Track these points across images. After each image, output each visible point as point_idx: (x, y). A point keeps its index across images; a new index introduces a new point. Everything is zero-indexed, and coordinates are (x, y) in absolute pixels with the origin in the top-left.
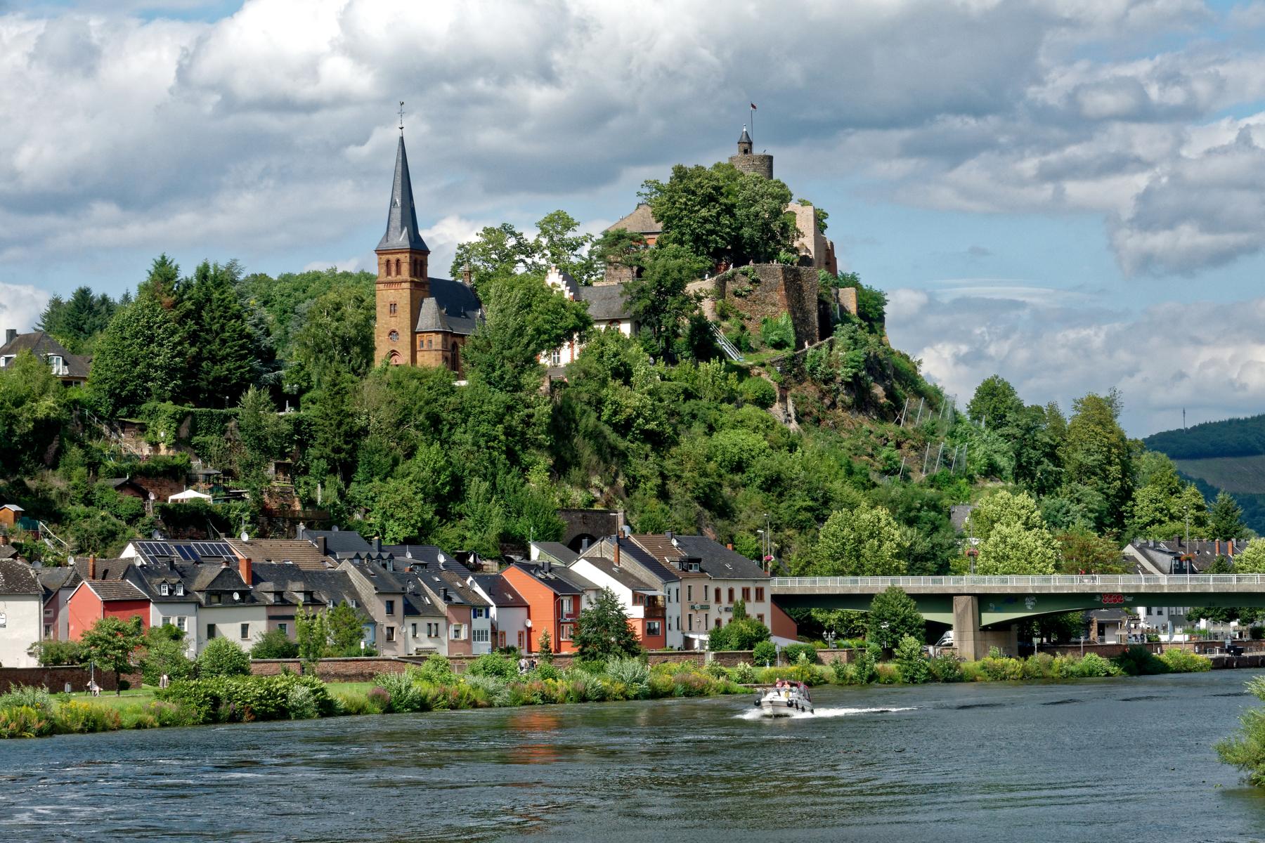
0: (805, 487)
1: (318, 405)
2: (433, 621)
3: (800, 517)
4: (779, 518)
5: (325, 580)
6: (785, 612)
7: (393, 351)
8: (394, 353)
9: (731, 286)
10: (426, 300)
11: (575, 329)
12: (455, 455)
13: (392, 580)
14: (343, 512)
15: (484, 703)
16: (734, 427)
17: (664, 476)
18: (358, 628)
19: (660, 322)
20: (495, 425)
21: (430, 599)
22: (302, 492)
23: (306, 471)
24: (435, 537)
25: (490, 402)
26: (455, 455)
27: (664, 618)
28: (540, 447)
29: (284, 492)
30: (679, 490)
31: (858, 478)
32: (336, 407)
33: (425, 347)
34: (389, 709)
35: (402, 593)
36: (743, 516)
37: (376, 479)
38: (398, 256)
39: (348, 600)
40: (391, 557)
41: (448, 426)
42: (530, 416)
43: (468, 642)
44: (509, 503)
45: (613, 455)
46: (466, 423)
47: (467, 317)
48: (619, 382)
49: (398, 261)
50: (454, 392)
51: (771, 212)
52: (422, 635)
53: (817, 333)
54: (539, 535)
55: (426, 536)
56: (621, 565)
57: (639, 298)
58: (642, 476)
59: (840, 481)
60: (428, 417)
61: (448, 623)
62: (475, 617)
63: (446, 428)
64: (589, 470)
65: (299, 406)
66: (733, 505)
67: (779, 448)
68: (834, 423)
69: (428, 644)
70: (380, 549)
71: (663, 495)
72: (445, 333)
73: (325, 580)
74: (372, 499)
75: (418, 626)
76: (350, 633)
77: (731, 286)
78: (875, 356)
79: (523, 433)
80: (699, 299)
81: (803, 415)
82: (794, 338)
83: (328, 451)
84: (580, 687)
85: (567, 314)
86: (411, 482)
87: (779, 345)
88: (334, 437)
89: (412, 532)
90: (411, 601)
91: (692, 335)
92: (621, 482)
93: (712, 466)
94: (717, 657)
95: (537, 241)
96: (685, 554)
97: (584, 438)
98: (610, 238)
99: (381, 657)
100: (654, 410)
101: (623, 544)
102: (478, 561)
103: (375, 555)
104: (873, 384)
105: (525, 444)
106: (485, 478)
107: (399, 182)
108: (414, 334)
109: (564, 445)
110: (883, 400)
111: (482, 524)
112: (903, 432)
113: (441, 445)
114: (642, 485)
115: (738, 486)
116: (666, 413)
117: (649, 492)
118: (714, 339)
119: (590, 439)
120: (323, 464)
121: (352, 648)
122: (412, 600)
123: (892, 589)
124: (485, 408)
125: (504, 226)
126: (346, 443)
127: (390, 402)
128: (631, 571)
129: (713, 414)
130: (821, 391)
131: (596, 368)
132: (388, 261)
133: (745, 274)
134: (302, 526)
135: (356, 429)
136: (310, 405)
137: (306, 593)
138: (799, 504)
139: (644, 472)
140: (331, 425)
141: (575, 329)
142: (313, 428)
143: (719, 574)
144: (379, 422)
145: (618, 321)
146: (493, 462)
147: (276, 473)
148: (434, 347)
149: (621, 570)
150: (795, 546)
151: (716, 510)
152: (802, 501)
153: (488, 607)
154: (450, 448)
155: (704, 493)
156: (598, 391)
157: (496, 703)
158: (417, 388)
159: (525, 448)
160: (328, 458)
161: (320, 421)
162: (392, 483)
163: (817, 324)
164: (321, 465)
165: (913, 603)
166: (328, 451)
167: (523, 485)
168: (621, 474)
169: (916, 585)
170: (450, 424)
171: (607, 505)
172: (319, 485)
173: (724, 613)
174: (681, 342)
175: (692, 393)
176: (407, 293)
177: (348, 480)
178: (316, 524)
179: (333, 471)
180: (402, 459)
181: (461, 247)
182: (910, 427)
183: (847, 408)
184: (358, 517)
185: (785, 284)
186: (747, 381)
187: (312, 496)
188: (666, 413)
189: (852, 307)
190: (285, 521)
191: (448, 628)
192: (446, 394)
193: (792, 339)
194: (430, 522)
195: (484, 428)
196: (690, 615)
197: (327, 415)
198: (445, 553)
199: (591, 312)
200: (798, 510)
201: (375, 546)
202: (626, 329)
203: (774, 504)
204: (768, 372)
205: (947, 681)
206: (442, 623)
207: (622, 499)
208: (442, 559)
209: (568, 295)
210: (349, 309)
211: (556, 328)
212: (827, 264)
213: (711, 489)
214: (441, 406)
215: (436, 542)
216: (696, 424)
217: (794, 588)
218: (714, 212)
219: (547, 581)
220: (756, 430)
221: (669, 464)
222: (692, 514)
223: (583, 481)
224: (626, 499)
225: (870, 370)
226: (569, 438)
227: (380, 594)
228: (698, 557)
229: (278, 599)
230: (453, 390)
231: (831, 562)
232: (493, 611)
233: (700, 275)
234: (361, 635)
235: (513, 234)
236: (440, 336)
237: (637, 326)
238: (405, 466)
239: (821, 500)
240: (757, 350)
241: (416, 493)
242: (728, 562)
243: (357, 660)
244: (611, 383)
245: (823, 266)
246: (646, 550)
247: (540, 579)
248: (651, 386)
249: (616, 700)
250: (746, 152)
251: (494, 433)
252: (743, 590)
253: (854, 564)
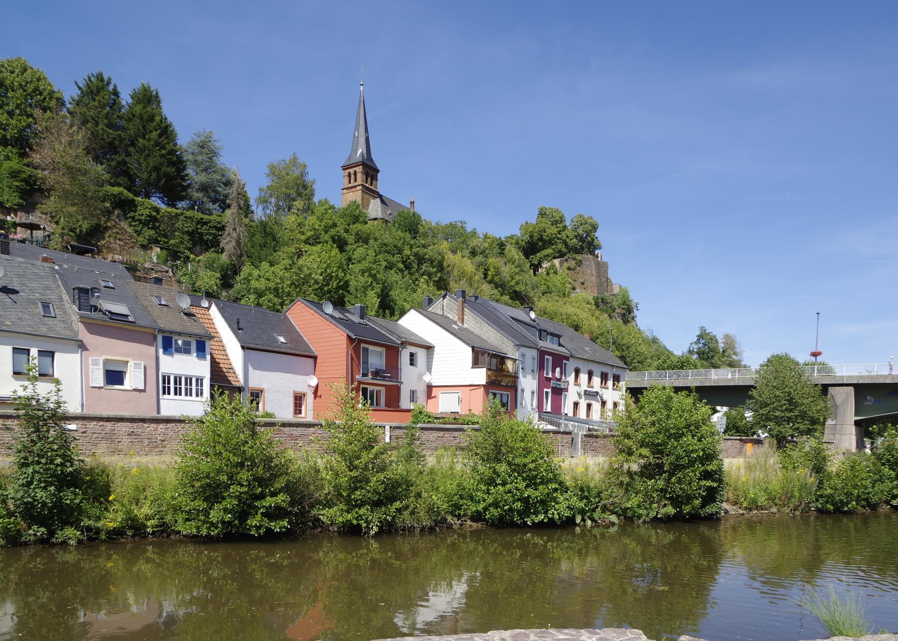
38: (355, 169)
56: (465, 326)
132: (349, 173)
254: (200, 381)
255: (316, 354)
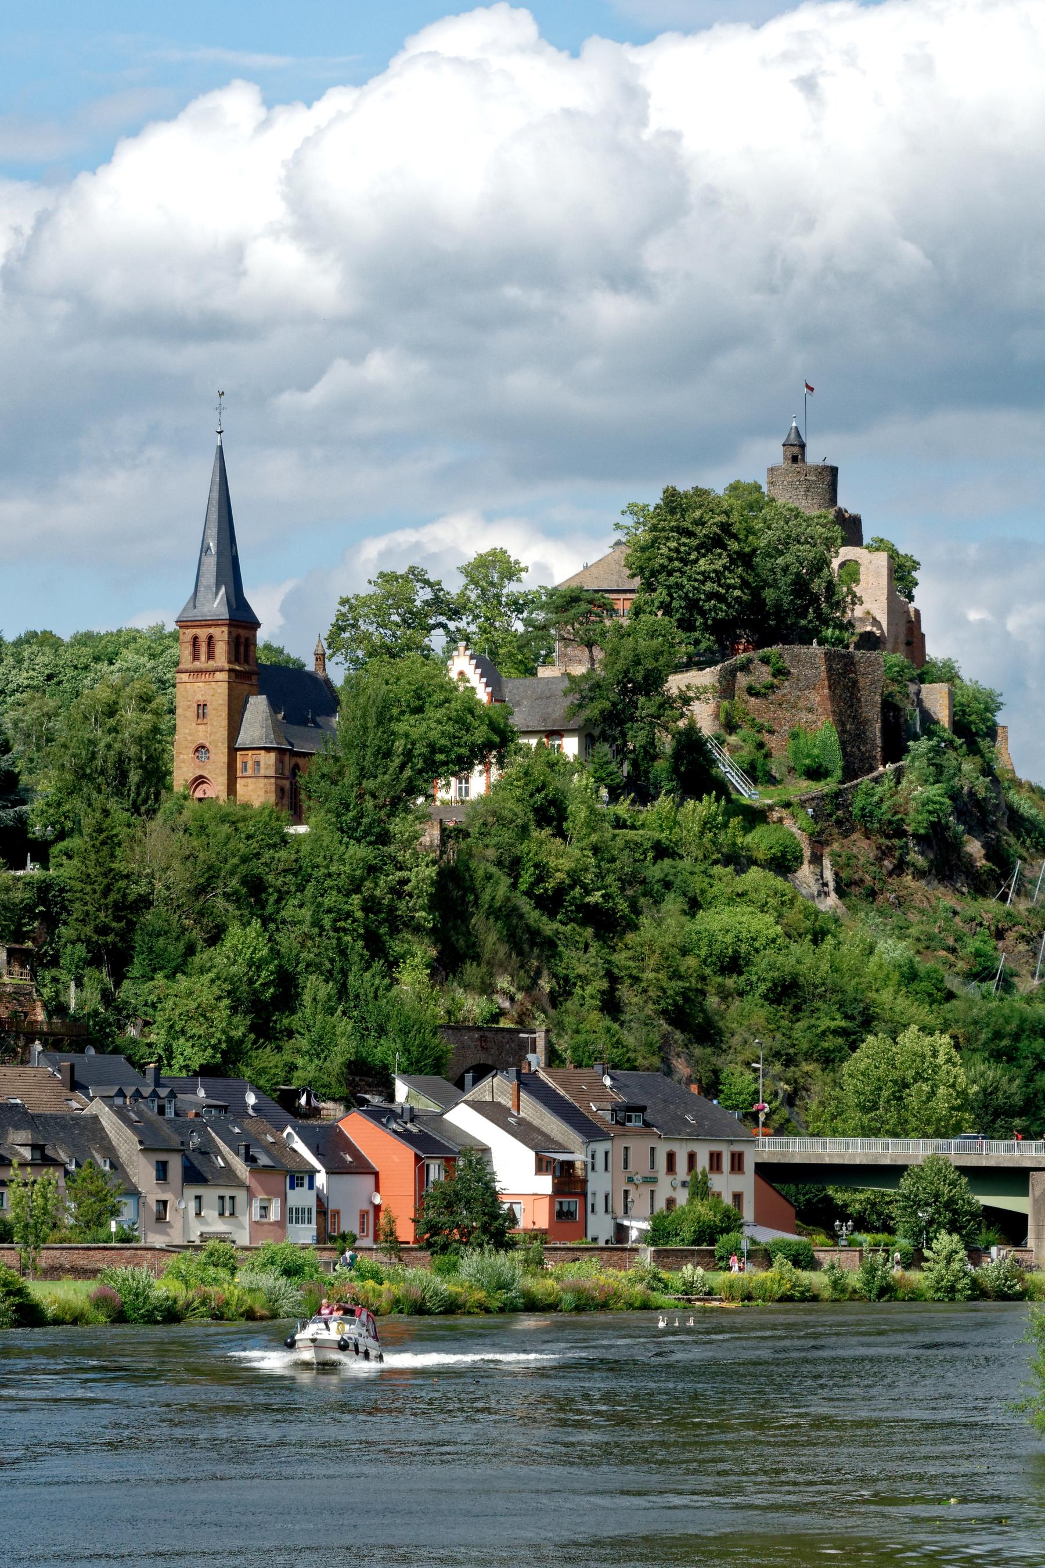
0: (836, 998)
1: (76, 862)
2: (227, 1193)
3: (826, 1045)
4: (793, 1046)
5: (64, 1127)
6: (774, 1188)
7: (201, 777)
8: (200, 780)
9: (743, 680)
10: (252, 700)
11: (489, 746)
12: (287, 940)
13: (166, 1130)
14: (110, 1025)
15: (265, 1312)
16: (731, 901)
17: (613, 979)
18: (111, 1200)
19: (623, 734)
20: (348, 895)
21: (224, 1159)
22: (47, 992)
23: (55, 962)
24: (247, 1066)
25: (341, 860)
26: (287, 940)
27: (584, 1194)
28: (418, 929)
29: (19, 993)
30: (635, 1000)
31: (925, 986)
32: (101, 865)
33: (249, 772)
34: (120, 1317)
35: (181, 1150)
36: (736, 1041)
37: (160, 975)
38: (211, 630)
39: (100, 1160)
40: (172, 1095)
41: (276, 896)
42: (405, 882)
43: (280, 1224)
44: (367, 1015)
45: (533, 944)
46: (302, 891)
47: (318, 726)
48: (548, 831)
49: (210, 638)
50: (286, 842)
51: (812, 565)
52: (210, 1213)
53: (879, 756)
54: (411, 1064)
55: (234, 1063)
56: (522, 1114)
57: (592, 699)
58: (579, 976)
59: (891, 989)
60: (244, 882)
61: (251, 1195)
62: (292, 1187)
63: (272, 899)
64: (493, 967)
65: (48, 861)
66: (721, 1024)
67: (800, 935)
68: (897, 898)
69: (219, 1226)
70: (158, 1083)
71: (611, 1006)
72: (280, 751)
73: (64, 1127)
74: (154, 1006)
75: (204, 1200)
76: (97, 1207)
77: (743, 680)
78: (972, 794)
79: (392, 909)
80: (687, 701)
81: (848, 885)
82: (841, 763)
83: (88, 930)
84: (416, 1293)
85: (476, 724)
86: (213, 981)
87: (815, 773)
88: (99, 910)
89: (213, 1057)
90: (196, 1163)
91: (677, 756)
92: (546, 985)
93: (691, 961)
94: (659, 1255)
95: (462, 594)
96: (622, 1099)
97: (487, 918)
98: (560, 602)
99: (142, 1244)
100: (600, 876)
101: (527, 1083)
102: (314, 1102)
103: (147, 1091)
104: (966, 837)
105: (396, 924)
106: (329, 976)
107: (214, 516)
108: (233, 751)
109: (455, 928)
110: (981, 863)
111: (320, 1048)
112: (1009, 914)
113: (264, 924)
114: (577, 990)
115: (731, 995)
116: (620, 879)
117: (589, 1002)
118: (713, 762)
119: (497, 919)
120: (81, 950)
121: (100, 1230)
122: (197, 1161)
123: (934, 1159)
124: (333, 869)
125: (412, 570)
126: (118, 919)
127: (187, 858)
128: (536, 1122)
129: (698, 883)
130: (879, 848)
131: (511, 810)
132: (195, 638)
133: (765, 661)
134: (38, 1046)
135: (131, 898)
136: (64, 860)
137: (34, 1147)
138: (825, 1023)
139: (582, 970)
140: (95, 892)
141: (489, 746)
142: (68, 896)
143: (674, 1129)
144: (168, 888)
145: (559, 733)
146: (343, 953)
147: (9, 963)
148: (262, 772)
149: (522, 1122)
150: (815, 1088)
151: (693, 1032)
152: (830, 1020)
153: (312, 1173)
154: (278, 929)
155: (675, 1004)
156: (513, 845)
157: (281, 1312)
158: (228, 838)
159: (394, 931)
160: (88, 941)
161: (79, 886)
162: (183, 983)
163: (879, 742)
164: (78, 953)
165: (964, 1180)
166: (88, 930)
167: (389, 988)
168: (545, 972)
169: (901, 1152)
170: (279, 891)
171: (520, 1021)
172: (72, 984)
173: (680, 1189)
174: (661, 766)
175: (667, 848)
176: (223, 689)
177: (119, 977)
178: (66, 1042)
179: (95, 962)
180: (200, 944)
181: (344, 602)
182: (1023, 906)
183: (920, 874)
184: (132, 1032)
185: (829, 678)
186: (760, 831)
187: (62, 999)
188: (620, 879)
189: (942, 714)
190: (18, 1038)
191: (250, 1204)
192: (274, 846)
193: (837, 764)
194: (241, 1042)
195: (328, 901)
196: (626, 1192)
197: (88, 876)
198: (258, 1089)
199: (518, 720)
200: (824, 1033)
201: (150, 1078)
202: (570, 746)
203: (785, 1023)
204: (794, 816)
205: (1003, 1296)
206: (241, 1196)
207: (544, 1012)
208: (251, 1099)
209: (483, 694)
210: (129, 714)
211: (459, 745)
212: (908, 644)
213: (687, 999)
214: (266, 864)
215: (248, 1072)
216: (670, 896)
217: (793, 1154)
218: (719, 565)
219: (406, 1137)
220: (763, 908)
221: (620, 958)
222: (655, 1037)
223: (483, 982)
224: (552, 1012)
225: (961, 814)
226: (465, 917)
227: (145, 1151)
228: (642, 1103)
229: (38, 1155)
230: (284, 840)
231: (859, 1114)
232: (321, 1179)
233: (691, 664)
234: (115, 1212)
235: (427, 582)
236: (272, 756)
237: (588, 741)
238: (205, 956)
239: (859, 1019)
240: (780, 782)
241: (219, 998)
242: (688, 1112)
243: (105, 1249)
244: (536, 834)
245: (902, 647)
246: (561, 1092)
247: (395, 1132)
248: (594, 838)
249: (469, 1313)
250: (795, 459)
251: (346, 907)
252: (712, 1155)
253: (892, 1116)
254: (310, 1210)
255: (378, 1169)
